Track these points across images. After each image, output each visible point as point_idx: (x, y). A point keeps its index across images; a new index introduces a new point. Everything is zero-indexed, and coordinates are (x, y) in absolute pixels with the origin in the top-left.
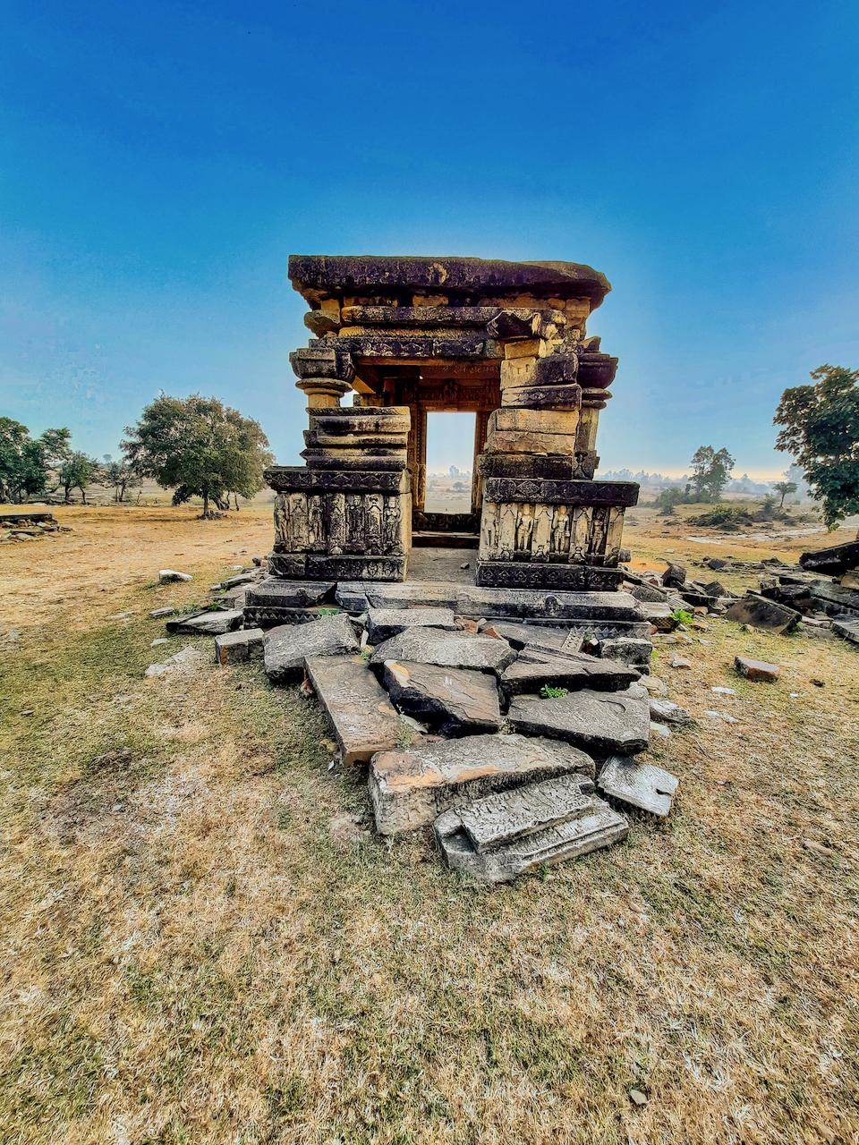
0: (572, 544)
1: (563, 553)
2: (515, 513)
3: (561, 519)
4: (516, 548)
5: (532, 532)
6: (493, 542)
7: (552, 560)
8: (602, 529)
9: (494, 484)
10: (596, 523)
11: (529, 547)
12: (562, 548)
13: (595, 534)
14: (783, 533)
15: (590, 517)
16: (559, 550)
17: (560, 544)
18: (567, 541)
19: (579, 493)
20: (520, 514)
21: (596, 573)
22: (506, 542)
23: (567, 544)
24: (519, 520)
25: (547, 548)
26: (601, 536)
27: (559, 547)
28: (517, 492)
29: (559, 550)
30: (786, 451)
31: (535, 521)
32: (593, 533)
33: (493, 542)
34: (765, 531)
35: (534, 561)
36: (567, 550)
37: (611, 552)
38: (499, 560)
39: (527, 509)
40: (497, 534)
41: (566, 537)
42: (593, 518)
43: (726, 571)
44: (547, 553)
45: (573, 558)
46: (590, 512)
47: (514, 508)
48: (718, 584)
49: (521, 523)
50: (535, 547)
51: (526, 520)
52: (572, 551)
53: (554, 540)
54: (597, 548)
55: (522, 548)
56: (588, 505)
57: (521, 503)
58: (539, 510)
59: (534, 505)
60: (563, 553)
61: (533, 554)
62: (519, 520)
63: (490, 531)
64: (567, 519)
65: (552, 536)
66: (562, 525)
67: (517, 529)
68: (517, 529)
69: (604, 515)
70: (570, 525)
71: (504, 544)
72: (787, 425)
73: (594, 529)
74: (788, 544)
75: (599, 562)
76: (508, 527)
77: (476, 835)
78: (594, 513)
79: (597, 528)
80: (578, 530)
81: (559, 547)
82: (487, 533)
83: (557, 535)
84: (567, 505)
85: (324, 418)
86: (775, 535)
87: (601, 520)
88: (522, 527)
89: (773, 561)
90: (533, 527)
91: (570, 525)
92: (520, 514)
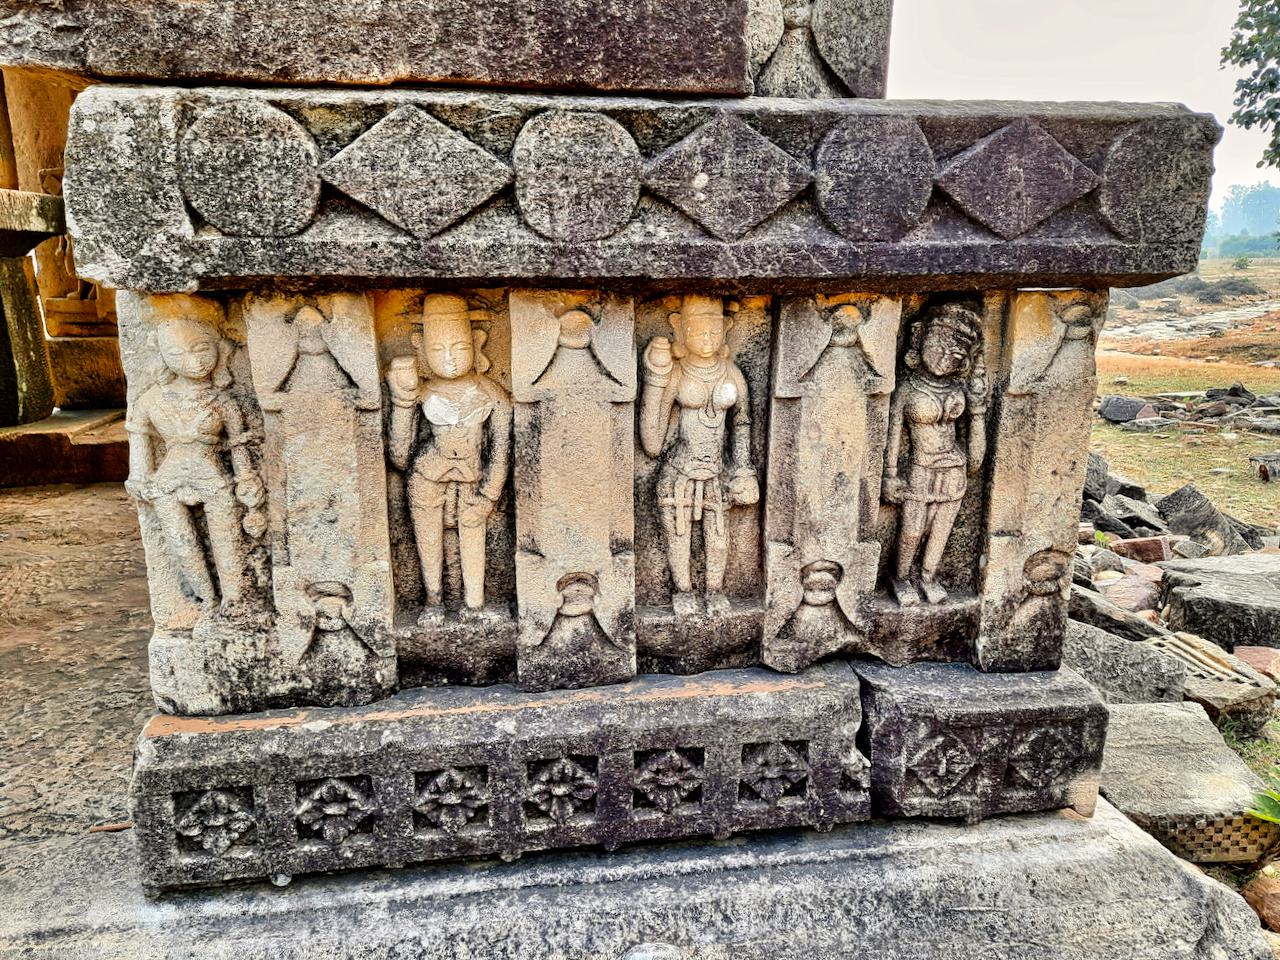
0: (775, 551)
1: (723, 609)
2: (363, 362)
3: (692, 393)
4: (411, 600)
5: (509, 490)
6: (231, 587)
7: (660, 661)
8: (962, 428)
9: (121, 142)
10: (926, 403)
11: (503, 589)
12: (714, 578)
13: (920, 476)
14: (1201, 319)
15: (884, 359)
16: (700, 590)
17: (699, 548)
18: (747, 524)
19: (806, 196)
20: (403, 374)
21: (937, 727)
22: (336, 572)
23: (746, 546)
24: (402, 421)
25: (616, 593)
26: (955, 484)
27: (699, 568)
28: (333, 200)
29: (700, 590)
30: (1255, 127)
31: (523, 417)
32: (906, 466)
33: (231, 587)
34: (1165, 316)
35: (547, 681)
36: (751, 588)
37: (1018, 581)
38: (298, 699)
39: (446, 334)
40: (254, 523)
41: (737, 508)
42: (902, 372)
43: (1147, 429)
44: (625, 619)
45: (787, 630)
46: (879, 327)
47: (350, 332)
48: (1195, 494)
49: (424, 435)
50: (535, 589)
51: (456, 413)
52: (783, 591)
53: (659, 529)
54: (933, 559)
55: (452, 598)
56: (861, 283)
57: (401, 289)
58: (535, 332)
59: (501, 307)
60: (723, 609)
61: (530, 637)
62: (402, 421)
63: (196, 514)
64: (731, 391)
65: (647, 499)
66: (703, 433)
67: (400, 472)
68: (400, 472)
69: (971, 344)
70: (754, 421)
71: (312, 590)
72: (1253, 65)
73: (911, 445)
74: (1219, 343)
75: (952, 644)
76: (324, 471)
77: (765, 638)
78: (908, 340)
79: (933, 439)
80: (807, 455)
81: (699, 568)
82: (178, 528)
83: (678, 503)
84: (728, 295)
85: (33, 76)
86: (1186, 325)
87: (952, 379)
88: (430, 466)
89: (1235, 392)
90: (510, 465)
91: (754, 421)
92: (403, 374)
